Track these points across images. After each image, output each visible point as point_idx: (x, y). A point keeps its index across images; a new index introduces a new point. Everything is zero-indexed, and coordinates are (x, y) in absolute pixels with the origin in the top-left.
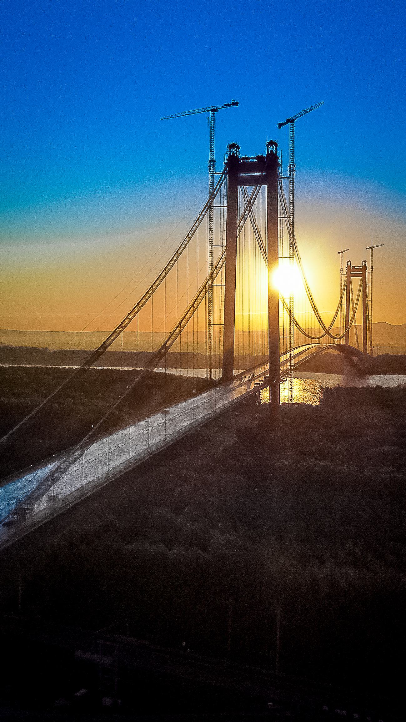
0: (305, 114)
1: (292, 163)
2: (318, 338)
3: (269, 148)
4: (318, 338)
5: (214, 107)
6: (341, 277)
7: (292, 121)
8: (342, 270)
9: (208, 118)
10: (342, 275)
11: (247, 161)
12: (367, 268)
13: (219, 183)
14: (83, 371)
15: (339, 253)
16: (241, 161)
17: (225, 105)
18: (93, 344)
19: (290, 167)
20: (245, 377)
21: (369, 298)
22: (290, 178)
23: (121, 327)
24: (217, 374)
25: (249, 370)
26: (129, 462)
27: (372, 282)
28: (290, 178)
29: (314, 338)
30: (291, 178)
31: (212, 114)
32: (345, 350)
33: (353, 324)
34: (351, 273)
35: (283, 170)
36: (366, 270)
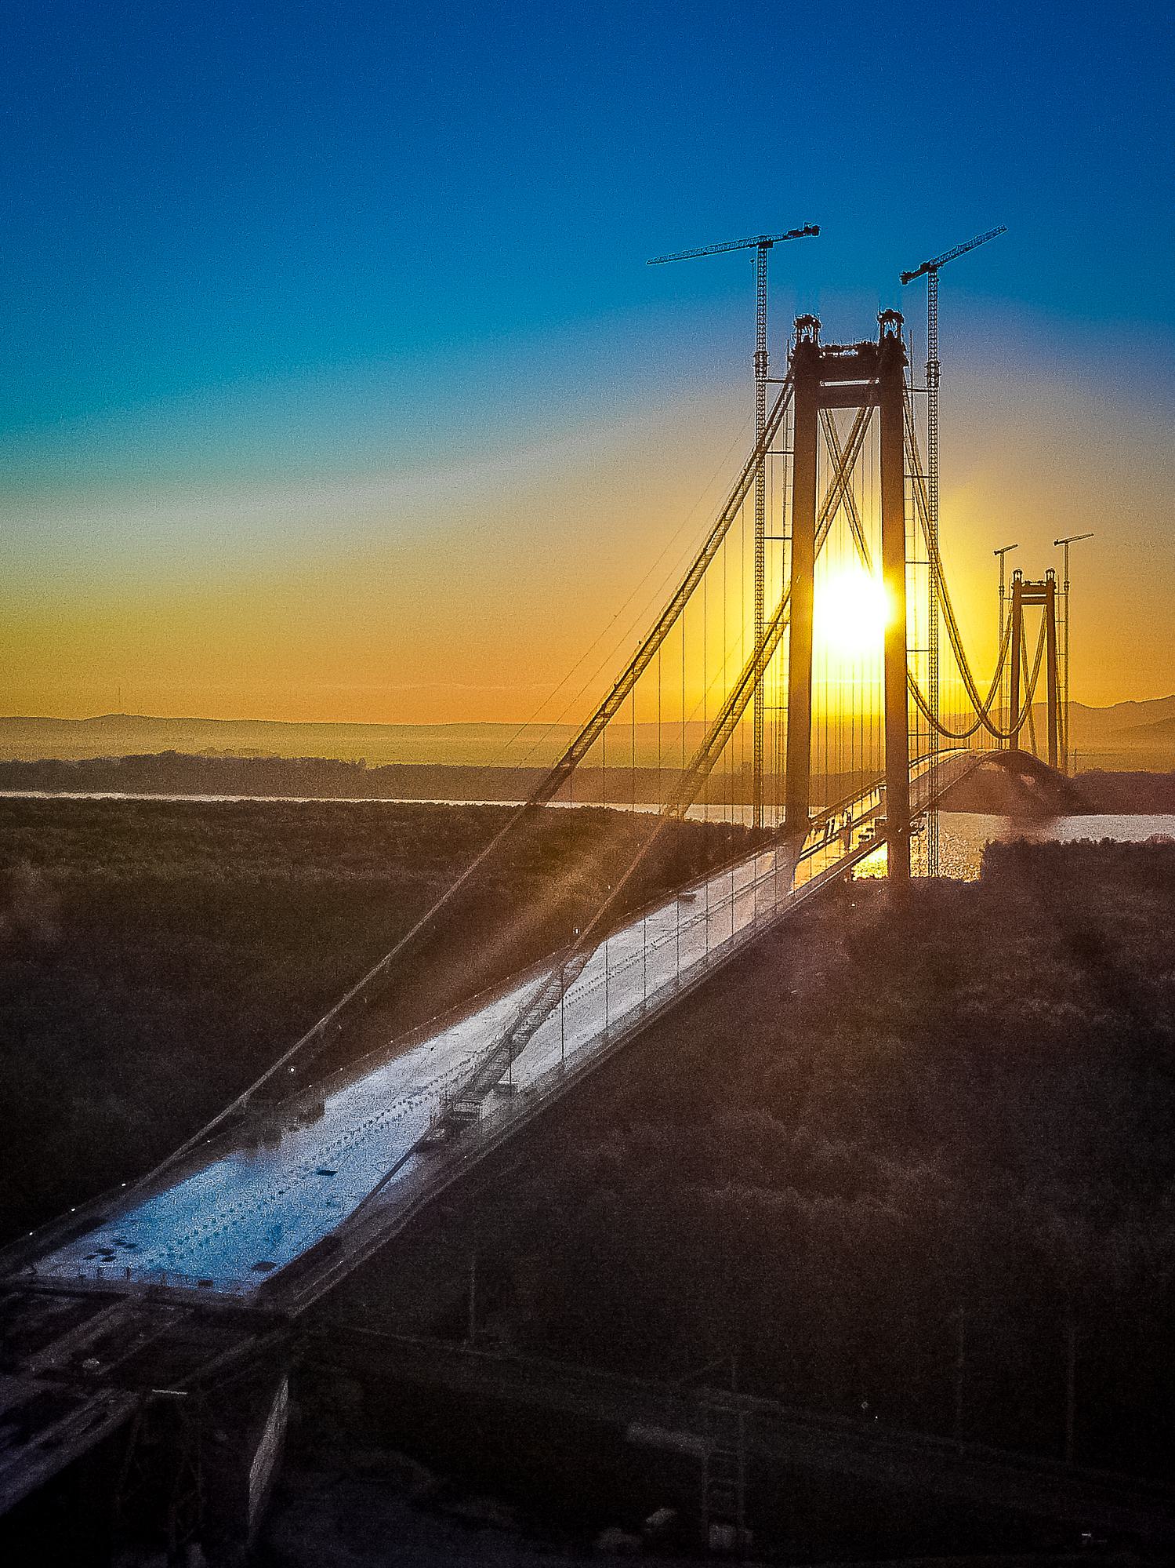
0: (962, 252)
1: (934, 358)
2: (964, 737)
3: (884, 326)
4: (964, 737)
5: (766, 237)
6: (1002, 604)
7: (933, 269)
8: (1002, 591)
9: (752, 261)
10: (1002, 599)
11: (837, 354)
12: (1056, 585)
13: (780, 401)
14: (532, 811)
15: (996, 553)
16: (822, 355)
17: (790, 233)
18: (548, 752)
19: (929, 367)
20: (833, 821)
21: (1060, 648)
22: (929, 391)
23: (602, 716)
24: (773, 817)
25: (839, 807)
26: (643, 1009)
27: (1067, 616)
28: (929, 391)
29: (955, 737)
30: (931, 391)
31: (761, 252)
32: (1016, 761)
33: (749, 713)
34: (1023, 596)
35: (914, 375)
36: (1055, 590)
